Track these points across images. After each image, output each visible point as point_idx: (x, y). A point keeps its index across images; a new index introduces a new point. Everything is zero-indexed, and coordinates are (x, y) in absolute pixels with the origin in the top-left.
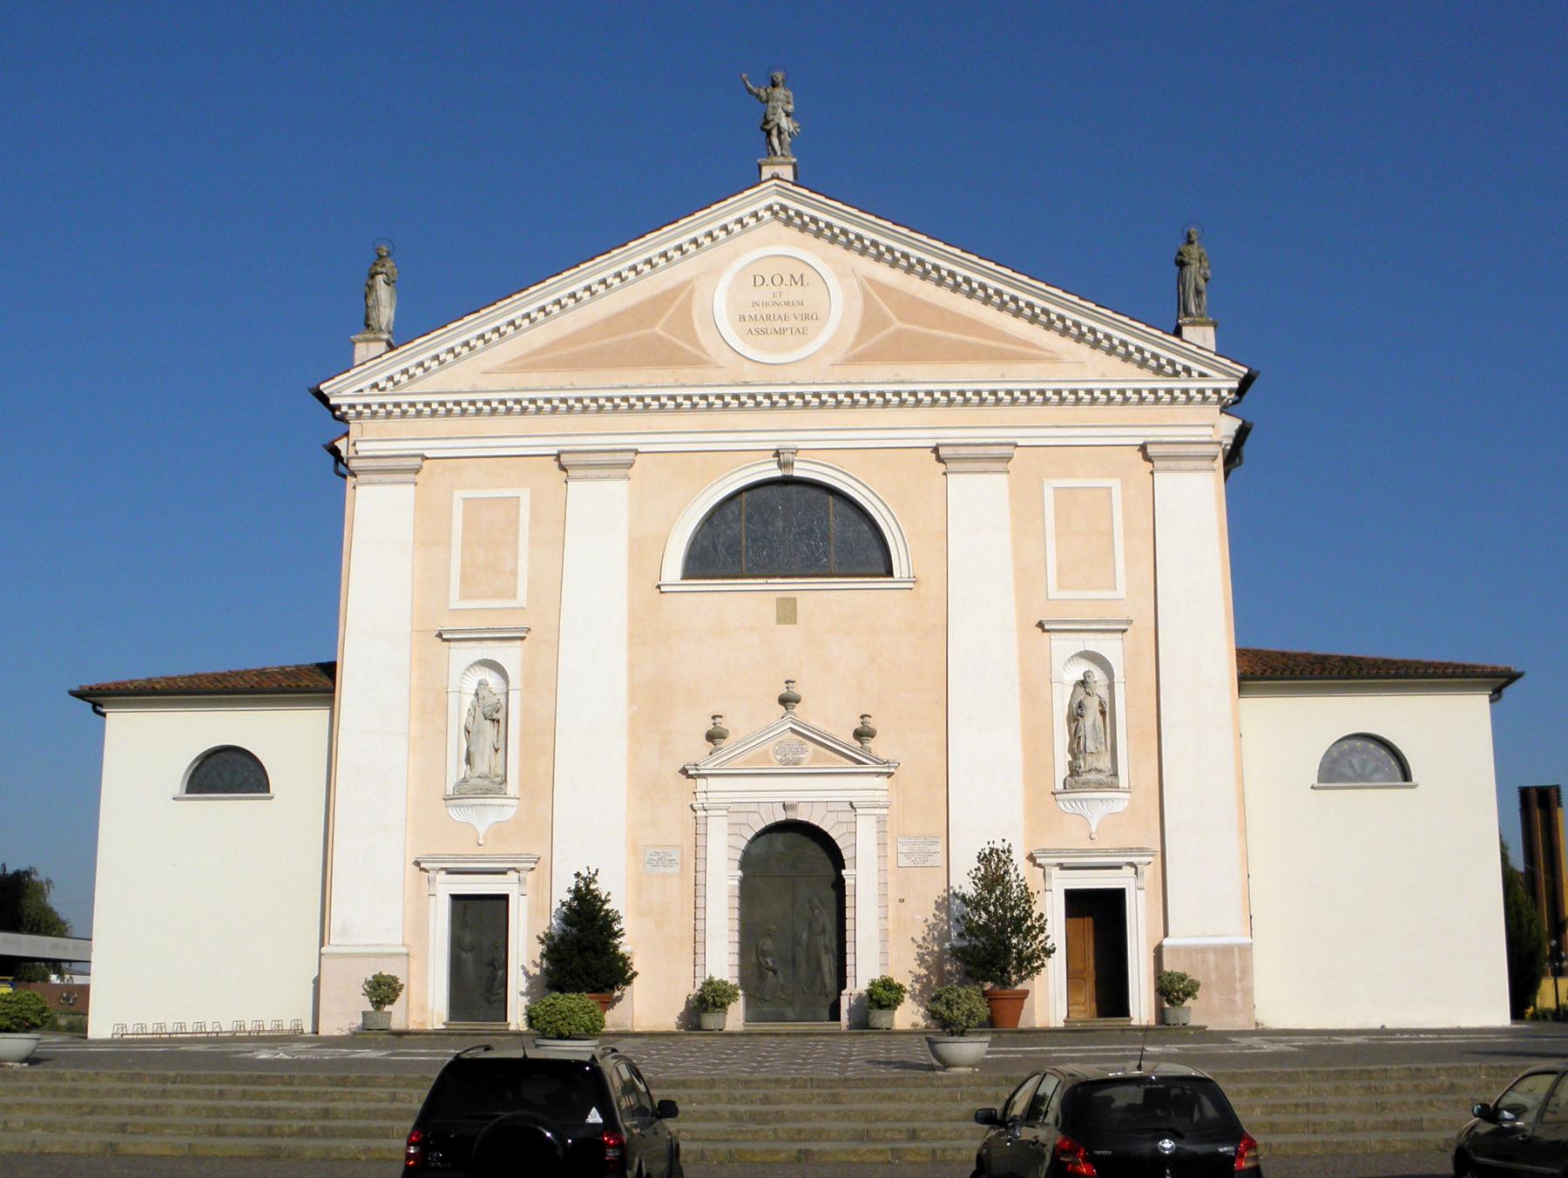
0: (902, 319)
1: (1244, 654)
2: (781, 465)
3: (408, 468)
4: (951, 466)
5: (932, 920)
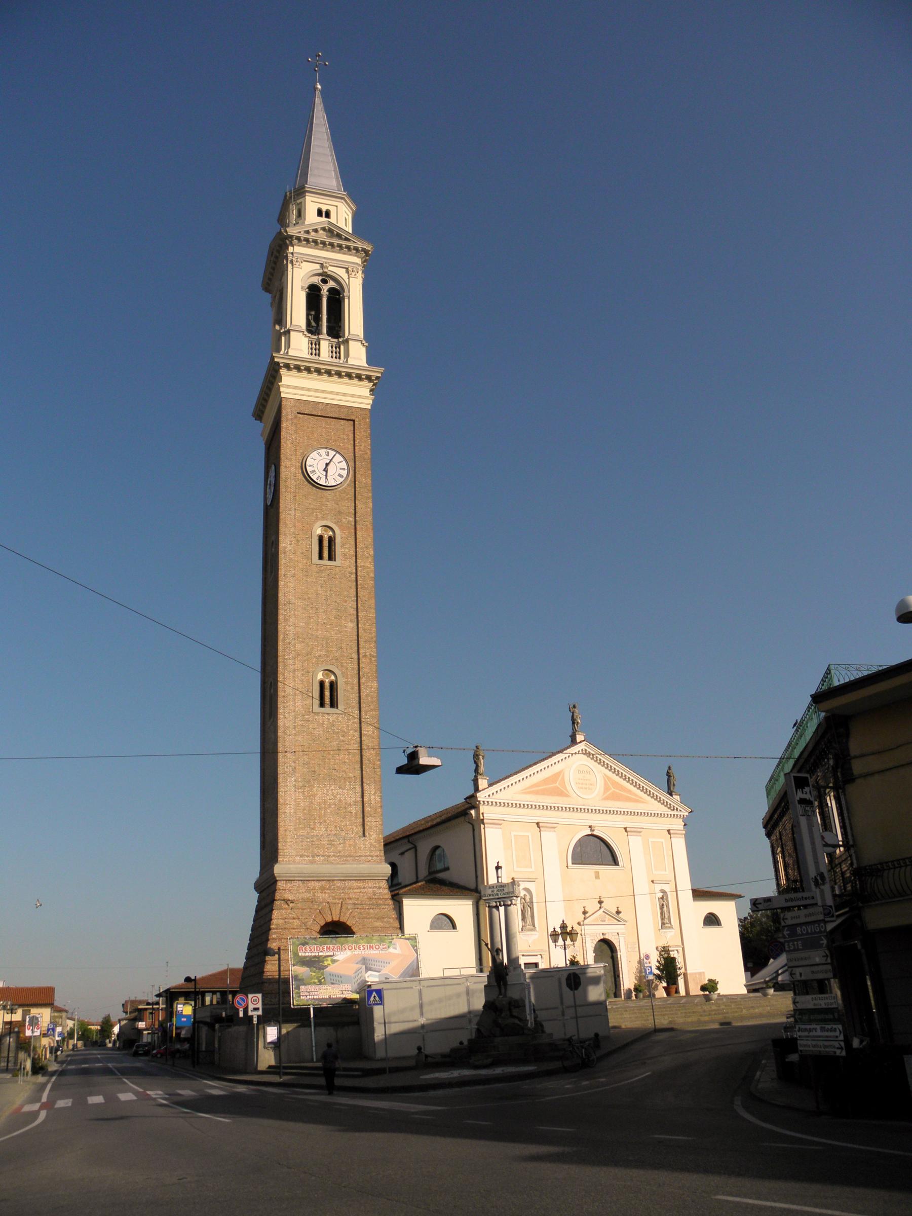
0: (614, 788)
1: (423, 888)
2: (591, 830)
3: (497, 823)
4: (629, 833)
5: (637, 967)
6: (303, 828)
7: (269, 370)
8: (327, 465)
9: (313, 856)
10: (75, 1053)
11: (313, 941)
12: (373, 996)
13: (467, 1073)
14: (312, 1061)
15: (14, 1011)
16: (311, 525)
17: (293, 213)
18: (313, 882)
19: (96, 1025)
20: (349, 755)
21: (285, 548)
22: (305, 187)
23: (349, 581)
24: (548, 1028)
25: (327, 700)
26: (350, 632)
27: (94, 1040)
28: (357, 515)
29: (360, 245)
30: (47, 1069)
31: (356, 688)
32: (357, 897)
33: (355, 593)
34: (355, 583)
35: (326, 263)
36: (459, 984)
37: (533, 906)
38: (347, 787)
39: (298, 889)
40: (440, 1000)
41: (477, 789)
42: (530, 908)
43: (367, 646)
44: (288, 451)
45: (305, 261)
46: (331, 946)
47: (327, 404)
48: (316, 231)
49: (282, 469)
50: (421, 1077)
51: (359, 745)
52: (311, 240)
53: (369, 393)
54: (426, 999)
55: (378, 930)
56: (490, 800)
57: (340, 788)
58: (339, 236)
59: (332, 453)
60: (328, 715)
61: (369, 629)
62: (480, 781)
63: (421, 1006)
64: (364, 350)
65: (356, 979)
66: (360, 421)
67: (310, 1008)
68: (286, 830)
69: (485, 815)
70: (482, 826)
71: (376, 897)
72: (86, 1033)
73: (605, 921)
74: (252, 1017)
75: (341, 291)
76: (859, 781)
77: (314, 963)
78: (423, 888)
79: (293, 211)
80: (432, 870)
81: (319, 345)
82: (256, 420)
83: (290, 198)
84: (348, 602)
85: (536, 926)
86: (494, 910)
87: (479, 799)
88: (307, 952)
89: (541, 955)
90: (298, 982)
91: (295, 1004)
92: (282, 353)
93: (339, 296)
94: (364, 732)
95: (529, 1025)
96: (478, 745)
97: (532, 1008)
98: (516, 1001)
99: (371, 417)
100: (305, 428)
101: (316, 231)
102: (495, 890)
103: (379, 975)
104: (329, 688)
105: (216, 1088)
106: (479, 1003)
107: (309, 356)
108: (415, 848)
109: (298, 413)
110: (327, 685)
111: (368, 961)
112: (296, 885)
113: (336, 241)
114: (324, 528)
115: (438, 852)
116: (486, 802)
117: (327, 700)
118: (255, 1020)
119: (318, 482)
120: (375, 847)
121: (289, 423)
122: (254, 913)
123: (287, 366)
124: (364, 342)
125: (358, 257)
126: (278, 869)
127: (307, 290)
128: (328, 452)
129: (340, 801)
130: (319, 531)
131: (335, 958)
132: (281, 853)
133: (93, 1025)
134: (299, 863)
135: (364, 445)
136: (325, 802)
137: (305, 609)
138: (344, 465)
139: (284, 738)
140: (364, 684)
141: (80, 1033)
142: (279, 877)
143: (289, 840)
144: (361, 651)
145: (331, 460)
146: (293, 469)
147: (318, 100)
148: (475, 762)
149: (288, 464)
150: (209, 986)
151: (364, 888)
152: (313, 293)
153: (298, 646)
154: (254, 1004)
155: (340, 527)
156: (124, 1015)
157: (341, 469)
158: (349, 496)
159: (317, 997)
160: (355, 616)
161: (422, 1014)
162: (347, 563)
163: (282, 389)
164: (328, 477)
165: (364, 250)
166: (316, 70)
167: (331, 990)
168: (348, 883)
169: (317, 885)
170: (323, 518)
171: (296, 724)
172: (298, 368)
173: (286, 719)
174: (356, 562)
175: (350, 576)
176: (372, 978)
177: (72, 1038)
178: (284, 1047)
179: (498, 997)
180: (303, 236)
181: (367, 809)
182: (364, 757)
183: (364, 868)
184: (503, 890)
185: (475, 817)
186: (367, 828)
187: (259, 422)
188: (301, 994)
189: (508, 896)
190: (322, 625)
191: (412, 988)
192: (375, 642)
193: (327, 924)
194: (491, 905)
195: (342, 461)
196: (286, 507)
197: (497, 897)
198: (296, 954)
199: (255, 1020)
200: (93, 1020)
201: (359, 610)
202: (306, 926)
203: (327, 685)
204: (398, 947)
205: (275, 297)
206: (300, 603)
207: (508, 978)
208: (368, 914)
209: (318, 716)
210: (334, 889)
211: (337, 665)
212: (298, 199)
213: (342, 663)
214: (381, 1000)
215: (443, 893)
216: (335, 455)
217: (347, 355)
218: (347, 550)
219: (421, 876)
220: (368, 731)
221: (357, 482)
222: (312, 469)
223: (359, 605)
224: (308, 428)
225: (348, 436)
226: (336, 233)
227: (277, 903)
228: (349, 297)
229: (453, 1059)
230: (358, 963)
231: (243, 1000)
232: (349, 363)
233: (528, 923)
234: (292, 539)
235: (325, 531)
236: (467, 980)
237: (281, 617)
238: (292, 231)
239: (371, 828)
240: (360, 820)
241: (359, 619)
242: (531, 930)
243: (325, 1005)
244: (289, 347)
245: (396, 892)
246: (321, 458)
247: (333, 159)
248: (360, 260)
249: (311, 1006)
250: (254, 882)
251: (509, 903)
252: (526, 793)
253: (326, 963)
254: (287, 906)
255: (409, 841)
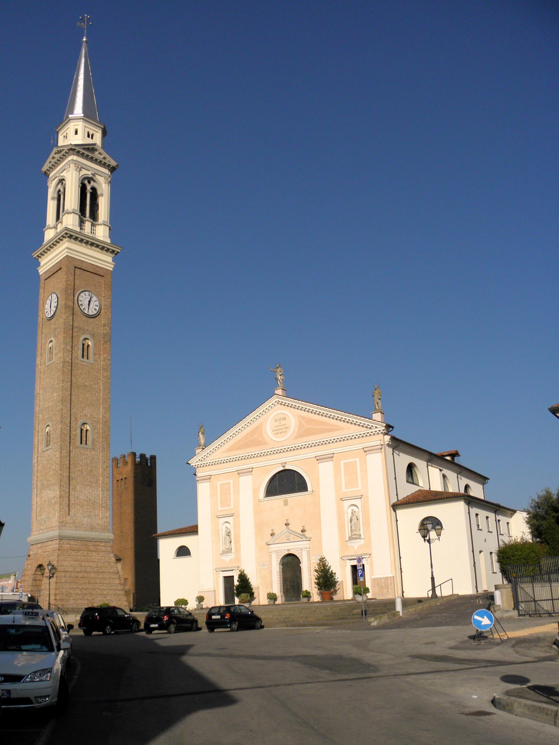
73: (289, 539)
76: (47, 625)
157: (96, 306)
185: (136, 635)
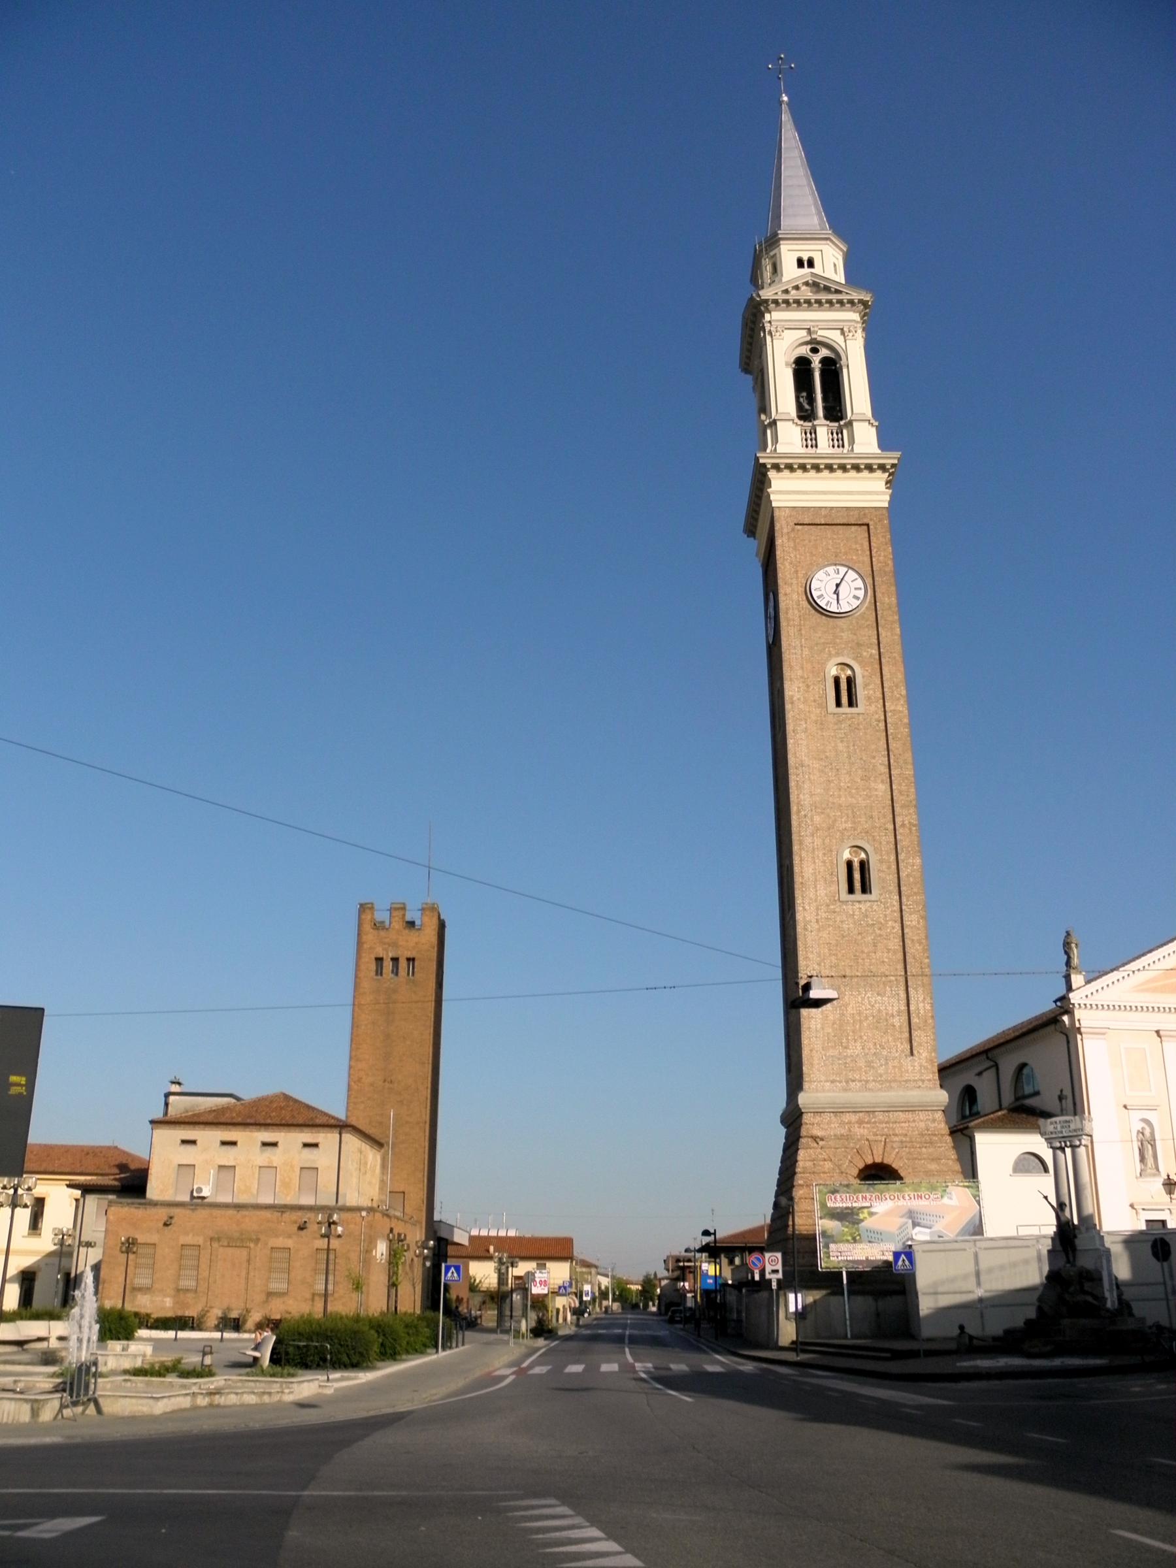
3: (1100, 1033)
6: (834, 1047)
7: (754, 475)
8: (838, 585)
9: (847, 1082)
10: (608, 1316)
11: (845, 1189)
12: (901, 1259)
13: (1016, 1362)
14: (846, 1337)
15: (515, 1265)
16: (823, 665)
17: (766, 269)
18: (848, 1114)
19: (636, 1284)
20: (888, 952)
21: (792, 696)
22: (777, 234)
23: (877, 731)
24: (1138, 1309)
25: (857, 885)
26: (882, 796)
27: (634, 1302)
28: (881, 645)
29: (856, 296)
30: (557, 1333)
31: (894, 867)
32: (904, 1132)
33: (885, 746)
34: (884, 734)
35: (813, 327)
36: (1028, 1247)
37: (1155, 1143)
38: (888, 993)
39: (829, 1123)
40: (1002, 1267)
41: (1069, 988)
42: (1152, 1145)
43: (905, 812)
44: (787, 573)
45: (786, 329)
46: (868, 1195)
47: (832, 508)
48: (797, 288)
49: (781, 598)
50: (958, 1364)
51: (901, 939)
52: (791, 301)
53: (884, 487)
54: (983, 1266)
55: (934, 1175)
56: (1088, 1002)
57: (878, 994)
58: (827, 289)
59: (843, 570)
60: (859, 903)
61: (906, 791)
62: (1073, 977)
63: (978, 1274)
64: (874, 430)
65: (900, 1237)
66: (876, 524)
67: (842, 1272)
68: (811, 1051)
69: (1081, 1022)
70: (1079, 1037)
71: (929, 1132)
72: (624, 1293)
74: (770, 1281)
75: (837, 360)
77: (847, 1216)
78: (1003, 1119)
79: (766, 267)
80: (1020, 1094)
81: (815, 433)
82: (748, 536)
83: (761, 251)
84: (877, 758)
85: (1160, 1170)
86: (1059, 1152)
87: (1072, 1001)
88: (838, 1202)
89: (1169, 1209)
90: (826, 1240)
91: (823, 1266)
92: (768, 451)
93: (836, 366)
94: (906, 923)
95: (1109, 1305)
96: (1069, 929)
97: (1114, 1282)
98: (1088, 1272)
99: (890, 518)
100: (807, 541)
101: (797, 288)
102: (1059, 1126)
103: (930, 1233)
104: (858, 869)
105: (717, 1363)
106: (1033, 1275)
107: (804, 450)
108: (996, 1066)
109: (795, 524)
110: (856, 865)
111: (915, 1215)
112: (827, 1117)
113: (824, 297)
114: (840, 666)
115: (1025, 1071)
116: (1082, 1005)
117: (857, 885)
118: (774, 1285)
119: (828, 609)
120: (926, 1068)
121: (785, 539)
122: (781, 1153)
123: (776, 467)
124: (872, 421)
125: (854, 312)
126: (803, 1099)
127: (794, 366)
128: (838, 570)
129: (879, 1011)
130: (834, 672)
131: (873, 1210)
132: (806, 1078)
133: (632, 1284)
134: (829, 1091)
135: (884, 555)
136: (860, 1014)
137: (822, 771)
138: (860, 583)
139: (805, 935)
140: (903, 861)
141: (617, 1293)
142: (804, 1108)
143: (816, 1062)
144: (898, 820)
145: (842, 579)
146: (795, 596)
147: (786, 117)
148: (1066, 953)
149: (788, 590)
150: (757, 1240)
151: (914, 1121)
152: (802, 368)
153: (817, 819)
154: (772, 1265)
155: (860, 663)
156: (665, 1274)
158: (868, 623)
159: (851, 1258)
160: (888, 776)
161: (979, 1284)
162: (873, 708)
163: (772, 497)
164: (840, 602)
165: (861, 301)
166: (780, 78)
167: (869, 1250)
168: (893, 1115)
169: (854, 1118)
170: (838, 654)
171: (819, 917)
172: (790, 467)
173: (805, 913)
174: (884, 706)
175: (878, 725)
176: (920, 1235)
177: (607, 1298)
178: (811, 1317)
179: (1065, 1267)
180: (781, 297)
181: (915, 1020)
182: (907, 954)
183: (914, 1095)
184: (1069, 1126)
186: (915, 1044)
187: (752, 539)
188: (831, 1254)
189: (1075, 1134)
190: (845, 790)
191: (965, 1250)
192: (915, 806)
193: (868, 1167)
194: (1054, 1145)
195: (856, 579)
196: (789, 645)
197: (1060, 1135)
198: (823, 1205)
199: (774, 1285)
200: (634, 1278)
201: (892, 767)
202: (840, 1169)
203: (856, 865)
204: (954, 1197)
205: (757, 378)
206: (816, 765)
207: (1077, 1242)
208: (920, 1153)
209: (846, 905)
210: (875, 1122)
211: (868, 839)
212: (772, 251)
213: (874, 836)
214: (912, 1266)
215: (1028, 1126)
216: (847, 572)
217: (852, 441)
218: (871, 692)
219: (1005, 1103)
220: (911, 921)
221: (878, 604)
222: (819, 593)
223: (892, 761)
224: (810, 541)
225: (862, 545)
226: (822, 286)
227: (802, 1141)
228: (848, 366)
229: (1008, 1342)
230: (902, 1217)
231: (758, 1259)
232: (855, 451)
233: (1149, 1165)
234: (801, 685)
235: (842, 670)
236: (1038, 1241)
237: (792, 784)
238: (766, 294)
239: (920, 1045)
240: (907, 1035)
241: (893, 778)
242: (1154, 1175)
243: (861, 1268)
244: (777, 442)
245: (965, 1125)
246: (829, 578)
247: (812, 189)
248: (858, 314)
249: (844, 1269)
250: (780, 1114)
251: (1078, 1143)
252: (1147, 990)
253: (861, 1216)
254: (815, 1145)
255: (988, 1058)
